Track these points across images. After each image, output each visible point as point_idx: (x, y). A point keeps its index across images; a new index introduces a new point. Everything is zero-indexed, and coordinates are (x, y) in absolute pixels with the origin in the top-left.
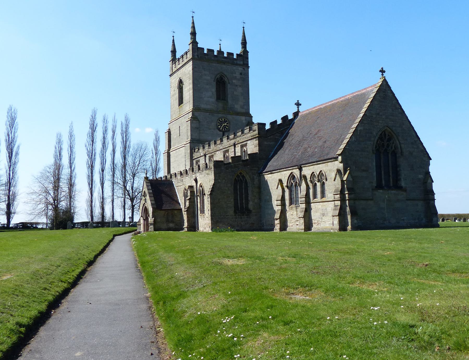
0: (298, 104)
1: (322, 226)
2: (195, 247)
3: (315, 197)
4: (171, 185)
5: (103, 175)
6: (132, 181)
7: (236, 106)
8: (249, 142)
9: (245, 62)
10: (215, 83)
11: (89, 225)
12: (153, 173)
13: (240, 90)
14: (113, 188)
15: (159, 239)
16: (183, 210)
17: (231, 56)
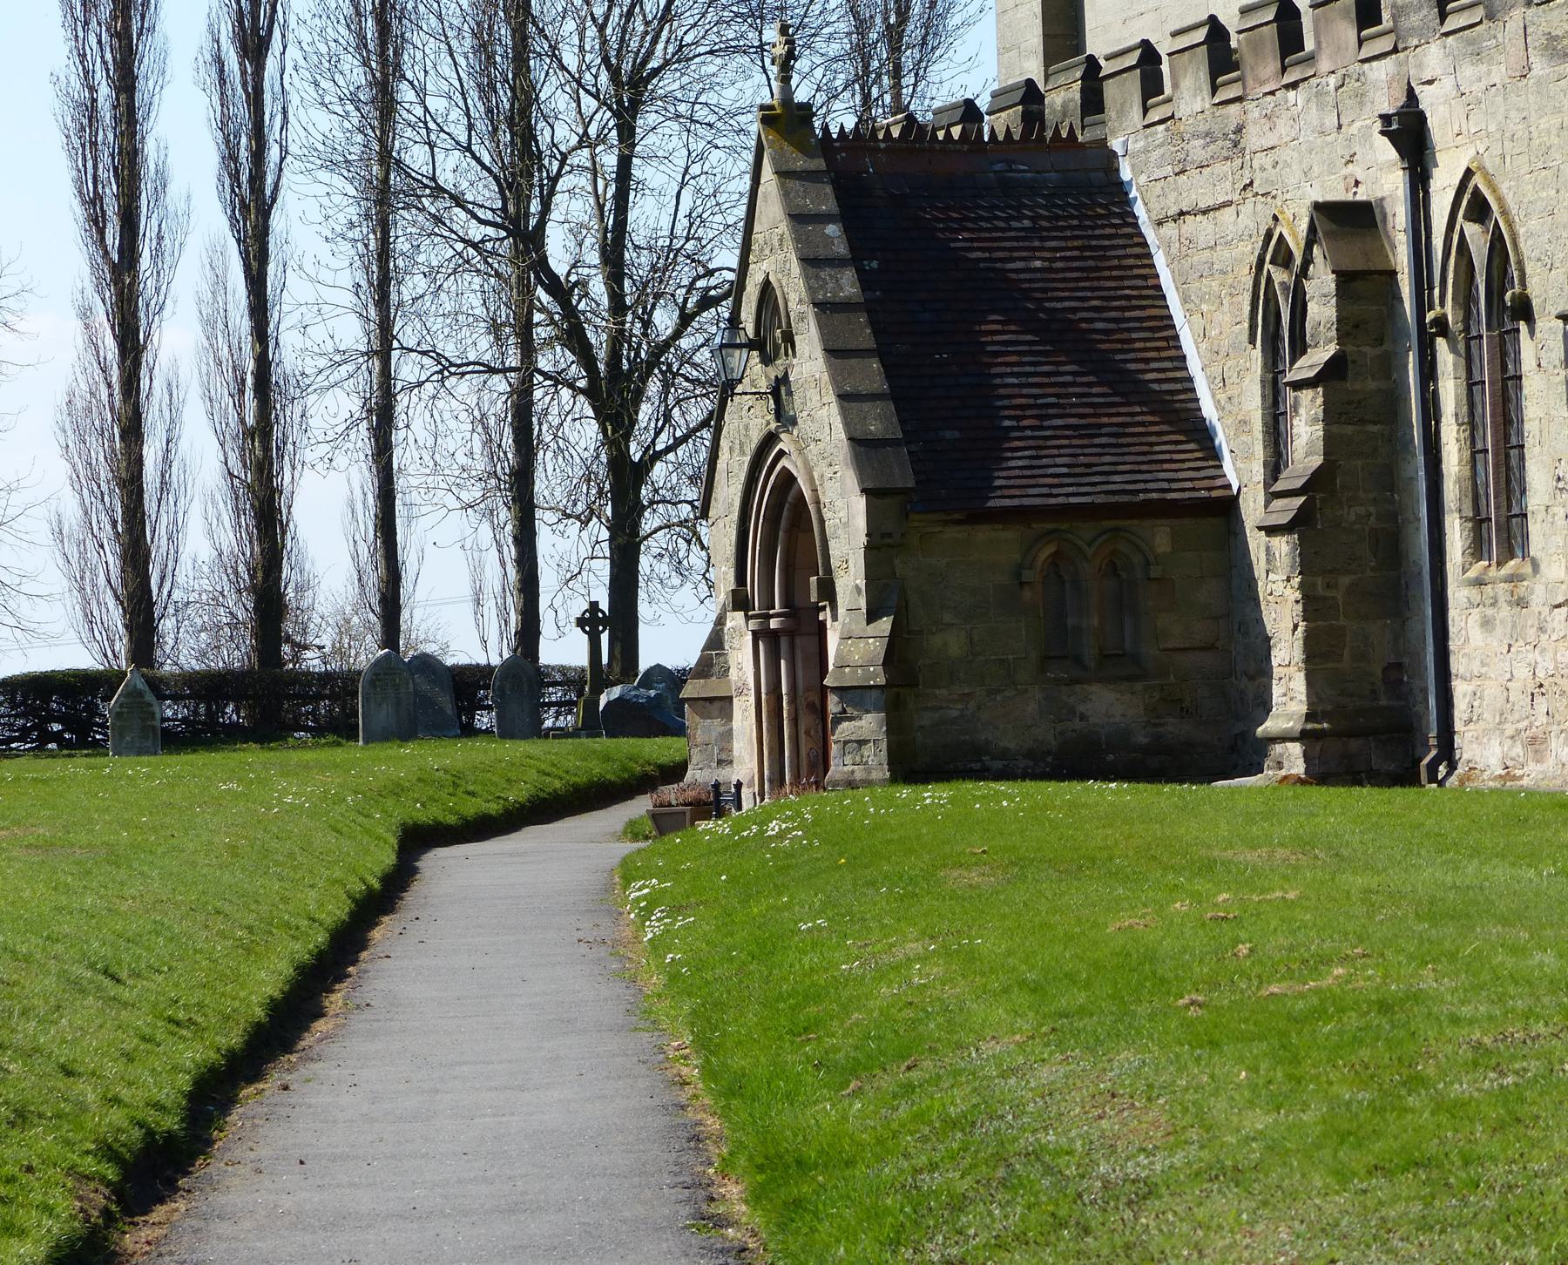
2: (1427, 980)
4: (1097, 192)
5: (256, 100)
6: (610, 160)
11: (108, 708)
12: (862, 52)
14: (384, 253)
15: (957, 879)
16: (1253, 509)
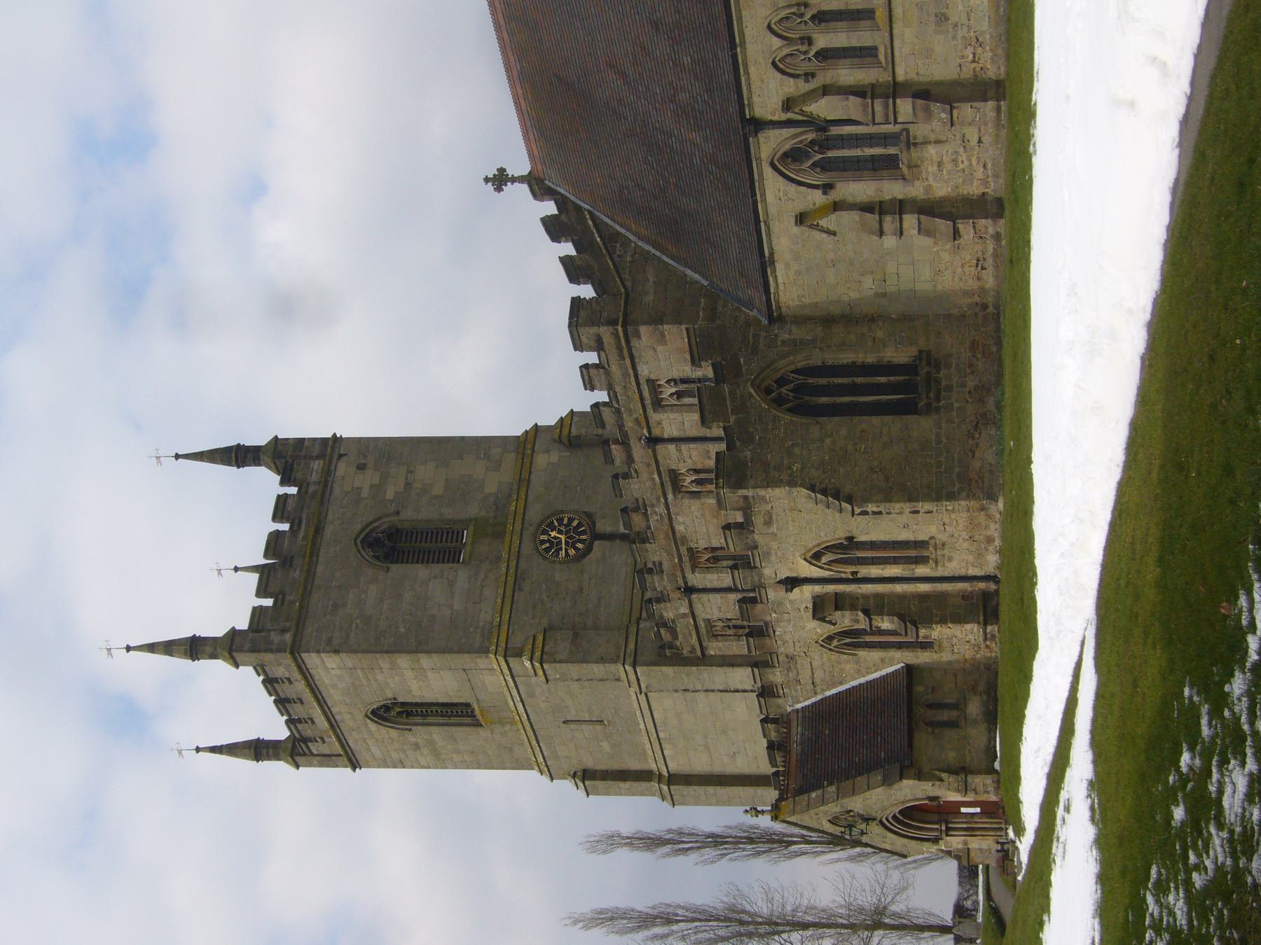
0: (500, 180)
1: (985, 26)
3: (865, 54)
7: (491, 488)
8: (644, 371)
9: (316, 450)
10: (394, 567)
13: (424, 471)
17: (291, 505)
